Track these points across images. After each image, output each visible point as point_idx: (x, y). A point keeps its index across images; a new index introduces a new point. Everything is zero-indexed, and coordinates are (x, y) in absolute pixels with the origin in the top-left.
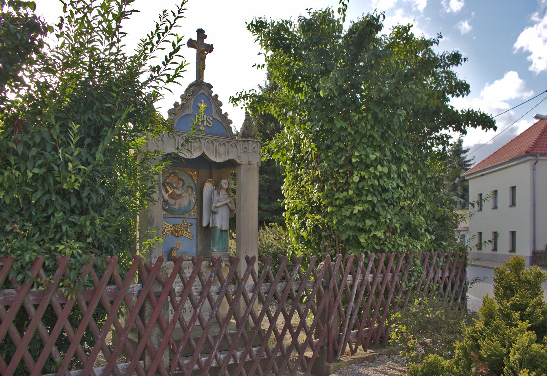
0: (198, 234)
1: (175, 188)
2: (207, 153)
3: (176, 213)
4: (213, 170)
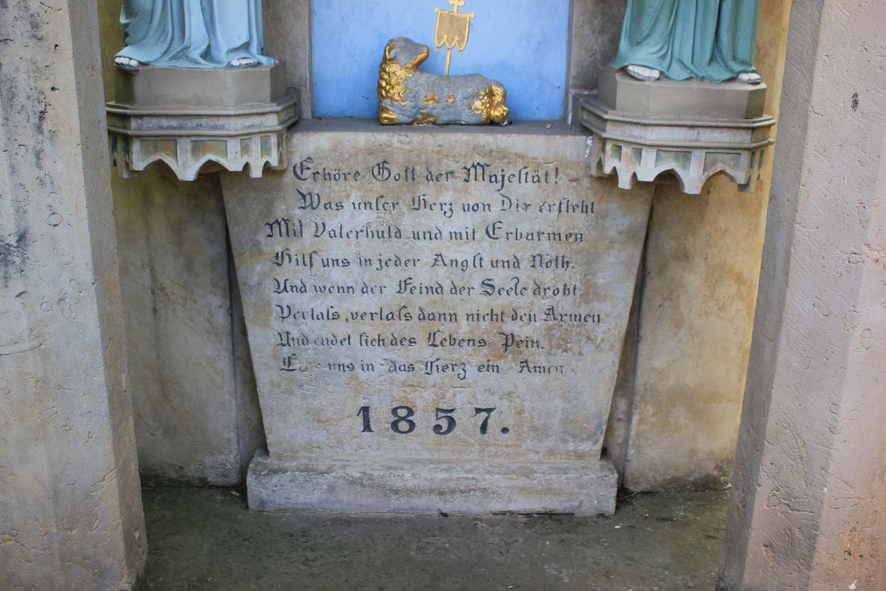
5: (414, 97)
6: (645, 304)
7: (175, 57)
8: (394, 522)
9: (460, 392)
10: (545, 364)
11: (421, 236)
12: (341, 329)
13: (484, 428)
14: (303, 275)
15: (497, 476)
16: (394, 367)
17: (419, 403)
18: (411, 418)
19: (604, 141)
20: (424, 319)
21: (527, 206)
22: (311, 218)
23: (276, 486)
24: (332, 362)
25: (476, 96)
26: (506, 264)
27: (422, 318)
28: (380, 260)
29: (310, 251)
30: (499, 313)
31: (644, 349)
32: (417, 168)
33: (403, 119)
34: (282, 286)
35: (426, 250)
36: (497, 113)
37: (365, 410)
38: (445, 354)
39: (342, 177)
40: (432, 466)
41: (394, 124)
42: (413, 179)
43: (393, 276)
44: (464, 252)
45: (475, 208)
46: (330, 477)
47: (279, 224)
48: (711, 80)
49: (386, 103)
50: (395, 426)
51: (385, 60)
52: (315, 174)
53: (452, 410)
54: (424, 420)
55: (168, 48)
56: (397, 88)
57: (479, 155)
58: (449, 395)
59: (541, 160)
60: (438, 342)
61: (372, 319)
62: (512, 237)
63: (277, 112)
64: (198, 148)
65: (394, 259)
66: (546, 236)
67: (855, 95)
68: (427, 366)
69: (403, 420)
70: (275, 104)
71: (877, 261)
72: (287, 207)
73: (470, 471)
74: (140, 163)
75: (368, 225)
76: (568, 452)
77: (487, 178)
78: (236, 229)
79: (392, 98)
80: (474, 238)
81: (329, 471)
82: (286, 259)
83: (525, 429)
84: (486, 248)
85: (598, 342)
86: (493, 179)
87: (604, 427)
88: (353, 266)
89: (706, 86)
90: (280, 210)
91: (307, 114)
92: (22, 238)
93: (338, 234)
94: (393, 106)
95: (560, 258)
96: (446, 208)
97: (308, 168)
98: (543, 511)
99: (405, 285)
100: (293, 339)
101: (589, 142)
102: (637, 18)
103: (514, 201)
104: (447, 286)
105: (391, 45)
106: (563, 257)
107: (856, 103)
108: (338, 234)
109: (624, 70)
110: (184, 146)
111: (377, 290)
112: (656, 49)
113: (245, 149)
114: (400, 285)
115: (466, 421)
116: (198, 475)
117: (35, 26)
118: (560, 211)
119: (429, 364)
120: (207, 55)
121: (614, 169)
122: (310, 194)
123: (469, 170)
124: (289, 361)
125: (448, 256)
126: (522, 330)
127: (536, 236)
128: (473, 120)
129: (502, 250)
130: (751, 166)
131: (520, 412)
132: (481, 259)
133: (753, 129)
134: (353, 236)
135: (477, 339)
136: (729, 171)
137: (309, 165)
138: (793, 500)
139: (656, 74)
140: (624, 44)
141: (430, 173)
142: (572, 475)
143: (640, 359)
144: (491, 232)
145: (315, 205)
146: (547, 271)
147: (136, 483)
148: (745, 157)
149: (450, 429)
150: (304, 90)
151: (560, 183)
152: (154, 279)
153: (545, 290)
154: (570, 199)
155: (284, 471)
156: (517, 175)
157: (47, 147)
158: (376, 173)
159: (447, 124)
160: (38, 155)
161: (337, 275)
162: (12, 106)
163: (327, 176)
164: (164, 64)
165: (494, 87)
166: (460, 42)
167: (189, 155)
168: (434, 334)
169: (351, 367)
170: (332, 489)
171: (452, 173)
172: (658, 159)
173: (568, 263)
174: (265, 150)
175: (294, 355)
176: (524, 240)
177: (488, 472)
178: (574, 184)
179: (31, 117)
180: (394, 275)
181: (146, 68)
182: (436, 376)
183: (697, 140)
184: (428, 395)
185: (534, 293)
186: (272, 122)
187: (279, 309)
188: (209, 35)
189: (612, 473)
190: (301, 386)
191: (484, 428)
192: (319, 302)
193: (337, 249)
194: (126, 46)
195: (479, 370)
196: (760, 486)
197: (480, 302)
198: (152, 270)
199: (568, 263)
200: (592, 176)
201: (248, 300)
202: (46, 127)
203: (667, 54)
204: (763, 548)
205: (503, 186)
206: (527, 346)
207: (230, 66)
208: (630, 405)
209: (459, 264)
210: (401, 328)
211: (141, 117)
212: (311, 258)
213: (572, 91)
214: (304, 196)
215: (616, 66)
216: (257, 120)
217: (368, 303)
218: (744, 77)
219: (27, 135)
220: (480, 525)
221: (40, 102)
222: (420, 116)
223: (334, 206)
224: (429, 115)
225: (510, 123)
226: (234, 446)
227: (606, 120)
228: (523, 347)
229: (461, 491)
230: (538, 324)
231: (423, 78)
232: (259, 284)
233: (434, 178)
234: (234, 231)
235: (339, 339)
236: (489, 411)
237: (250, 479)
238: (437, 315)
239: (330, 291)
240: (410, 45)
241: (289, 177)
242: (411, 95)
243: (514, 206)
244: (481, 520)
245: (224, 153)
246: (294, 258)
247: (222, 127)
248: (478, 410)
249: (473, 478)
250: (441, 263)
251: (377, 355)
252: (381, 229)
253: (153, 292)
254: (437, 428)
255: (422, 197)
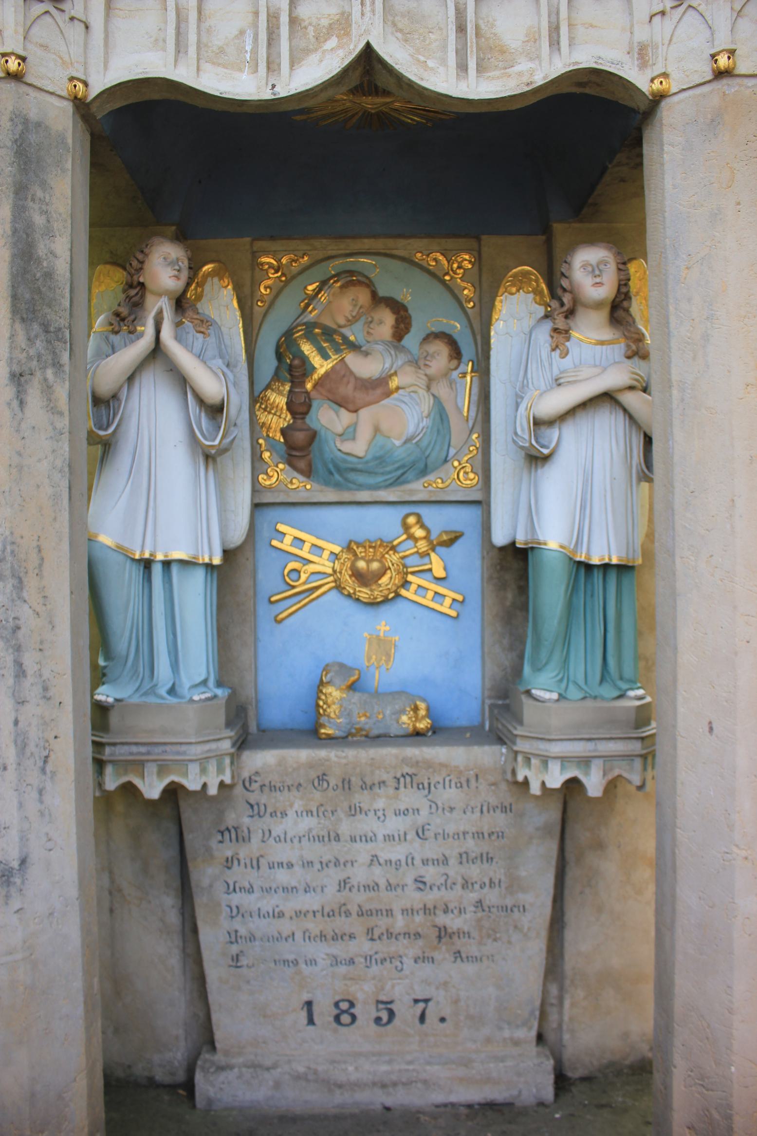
0: (485, 585)
1: (354, 347)
2: (395, 54)
3: (361, 479)
4: (557, 227)
5: (348, 715)
6: (567, 892)
7: (145, 694)
8: (338, 1118)
9: (399, 984)
10: (477, 954)
11: (358, 839)
12: (285, 926)
13: (422, 1018)
14: (250, 877)
15: (436, 1067)
16: (336, 961)
17: (360, 996)
18: (352, 1011)
19: (516, 753)
20: (362, 915)
21: (452, 809)
22: (258, 826)
23: (223, 1083)
24: (277, 957)
25: (403, 711)
26: (436, 862)
27: (361, 914)
28: (321, 863)
29: (258, 855)
30: (432, 907)
31: (569, 935)
32: (353, 779)
33: (338, 733)
34: (231, 887)
35: (362, 852)
36: (421, 726)
37: (309, 1004)
38: (384, 948)
39: (286, 788)
40: (374, 1059)
41: (332, 740)
42: (349, 788)
43: (334, 875)
44: (397, 852)
45: (406, 812)
46: (276, 1073)
47: (229, 831)
48: (603, 699)
49: (323, 720)
50: (337, 1019)
51: (322, 683)
52: (262, 786)
53: (391, 1002)
54: (365, 1012)
55: (139, 687)
56: (334, 707)
57: (407, 765)
58: (388, 987)
59: (462, 768)
60: (376, 936)
61: (314, 916)
62: (440, 838)
63: (230, 738)
64: (163, 770)
65: (333, 860)
66: (471, 835)
67: (710, 723)
68: (366, 959)
69: (345, 1013)
70: (228, 730)
71: (746, 858)
72: (237, 816)
73: (410, 1063)
74: (111, 783)
75: (310, 830)
76: (505, 1040)
77: (415, 786)
78: (191, 836)
79: (329, 716)
80: (405, 839)
81: (275, 1066)
82: (236, 862)
83: (462, 1018)
84: (416, 848)
85: (525, 930)
86: (421, 786)
87: (537, 1013)
88: (297, 869)
89: (599, 704)
90: (231, 819)
91: (253, 728)
92: (23, 862)
93: (282, 839)
94: (330, 722)
95: (485, 855)
96: (380, 814)
97: (256, 781)
98: (483, 1101)
99: (344, 884)
100: (241, 937)
101: (504, 750)
102: (537, 646)
103: (440, 805)
104: (383, 883)
105: (326, 669)
106: (488, 854)
107: (711, 729)
108: (282, 839)
109: (528, 693)
110: (151, 769)
111: (319, 890)
112: (554, 674)
113: (203, 771)
114: (340, 885)
115: (406, 1012)
116: (146, 1074)
117: (46, 689)
118: (482, 812)
119: (368, 958)
120: (172, 691)
121: (526, 778)
122: (258, 804)
123: (399, 780)
124: (236, 958)
125: (383, 856)
126: (454, 922)
127: (461, 836)
128: (401, 733)
129: (432, 850)
130: (645, 769)
131: (456, 1001)
132: (413, 859)
133: (642, 739)
134: (296, 841)
135: (412, 932)
136: (625, 775)
137: (257, 779)
138: (706, 1080)
139: (555, 696)
140: (527, 669)
141: (365, 783)
142: (510, 1063)
143: (566, 945)
144: (421, 833)
145: (262, 813)
146: (473, 867)
147: (100, 1083)
148: (638, 763)
149: (390, 1020)
150: (250, 707)
151: (481, 787)
152: (112, 881)
153: (472, 884)
154: (491, 801)
155: (229, 1067)
156: (441, 782)
157: (49, 785)
158: (316, 784)
159: (378, 737)
160: (41, 792)
161: (282, 877)
162: (23, 754)
163: (273, 788)
164: (136, 700)
165: (418, 703)
166: (388, 661)
167: (155, 777)
168: (372, 929)
169: (296, 963)
170: (277, 1085)
171: (384, 782)
172: (563, 768)
173: (492, 858)
174: (220, 770)
175: (242, 952)
176: (451, 839)
177: (429, 1063)
178: (493, 788)
179: (38, 762)
180: (334, 875)
181: (120, 704)
182: (375, 969)
183: (595, 750)
184: (368, 987)
185: (463, 888)
186: (226, 746)
187: (228, 909)
188: (173, 672)
189: (548, 1059)
190: (248, 982)
191: (422, 1018)
192: (265, 902)
193: (282, 853)
194: (103, 684)
195: (416, 961)
196: (675, 1067)
197: (414, 897)
198: (111, 872)
199: (492, 858)
200: (507, 781)
201: (200, 901)
202: (49, 768)
203: (564, 677)
204: (687, 1131)
205: (429, 792)
206: (459, 937)
207: (191, 701)
208: (561, 989)
209: (393, 864)
210: (341, 924)
211: (114, 744)
212: (258, 861)
213: (488, 702)
214: (252, 806)
215: (522, 689)
216: (213, 746)
217: (311, 902)
218: (631, 693)
219: (34, 777)
220: (423, 1118)
221: (45, 749)
222: (353, 731)
223: (279, 814)
224: (361, 729)
225: (434, 732)
226: (182, 1044)
227: (516, 736)
228: (455, 938)
229: (404, 1084)
230: (468, 916)
231: (356, 697)
232: (211, 886)
233: (368, 787)
234: (188, 837)
235: (284, 936)
236: (426, 1001)
237: (199, 1077)
238: (374, 912)
239: (275, 891)
240: (343, 668)
241: (239, 790)
242: (345, 713)
243: (440, 810)
244: (424, 1113)
245: (185, 775)
246: (242, 862)
247: (184, 753)
248: (416, 1001)
249: (414, 1070)
250: (376, 862)
251: (320, 951)
252: (321, 833)
253: (110, 893)
254: (378, 1020)
255: (358, 805)
